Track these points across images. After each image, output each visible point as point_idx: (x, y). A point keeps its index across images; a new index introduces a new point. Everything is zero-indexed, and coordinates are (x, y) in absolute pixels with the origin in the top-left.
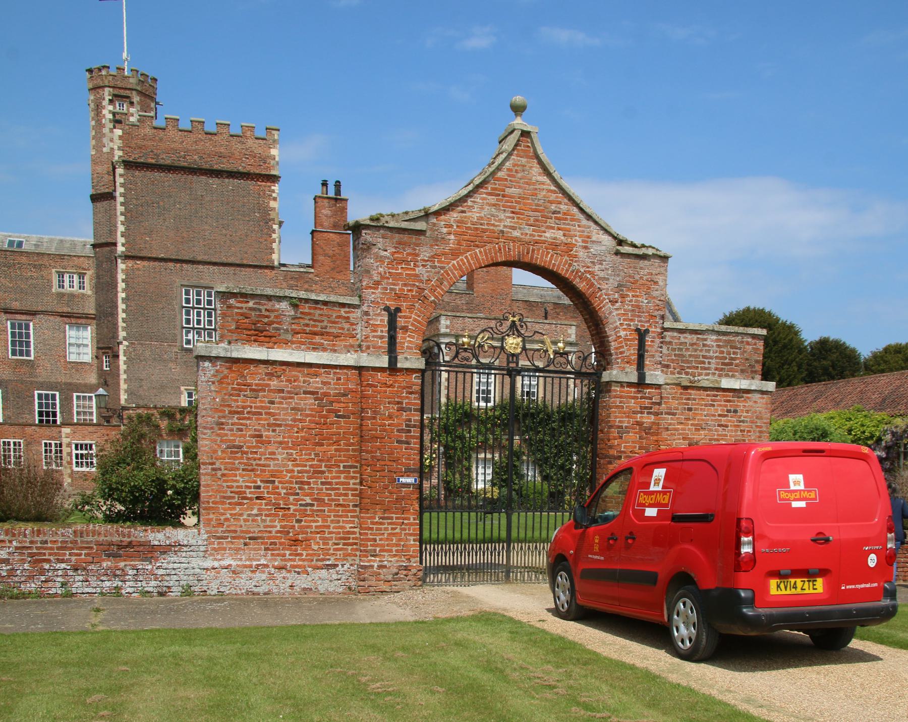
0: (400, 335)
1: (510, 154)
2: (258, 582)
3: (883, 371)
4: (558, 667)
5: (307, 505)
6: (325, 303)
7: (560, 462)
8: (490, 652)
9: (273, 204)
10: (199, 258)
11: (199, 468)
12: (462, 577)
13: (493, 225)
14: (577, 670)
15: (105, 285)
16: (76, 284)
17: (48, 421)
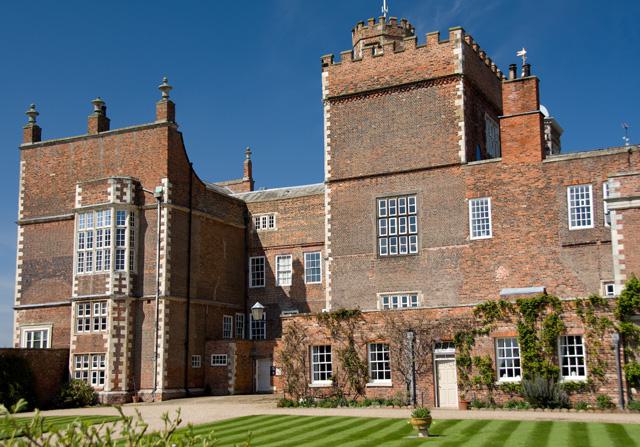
10: (392, 170)
17: (322, 351)
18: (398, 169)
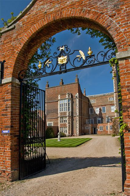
13: (42, 12)
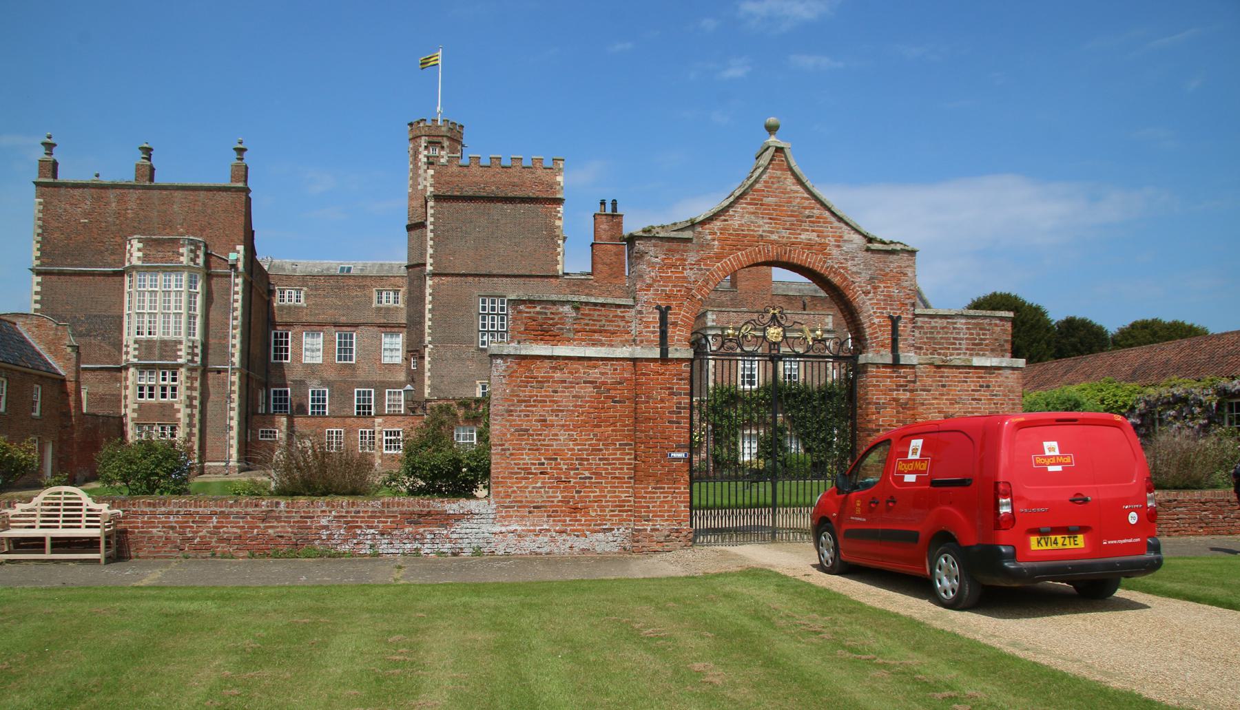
0: (670, 330)
1: (766, 168)
2: (542, 544)
3: (1131, 346)
4: (823, 615)
5: (586, 478)
6: (603, 305)
7: (822, 436)
8: (757, 602)
9: (558, 223)
11: (490, 449)
12: (731, 538)
14: (842, 618)
15: (415, 300)
16: (392, 300)
18: (500, 272)
